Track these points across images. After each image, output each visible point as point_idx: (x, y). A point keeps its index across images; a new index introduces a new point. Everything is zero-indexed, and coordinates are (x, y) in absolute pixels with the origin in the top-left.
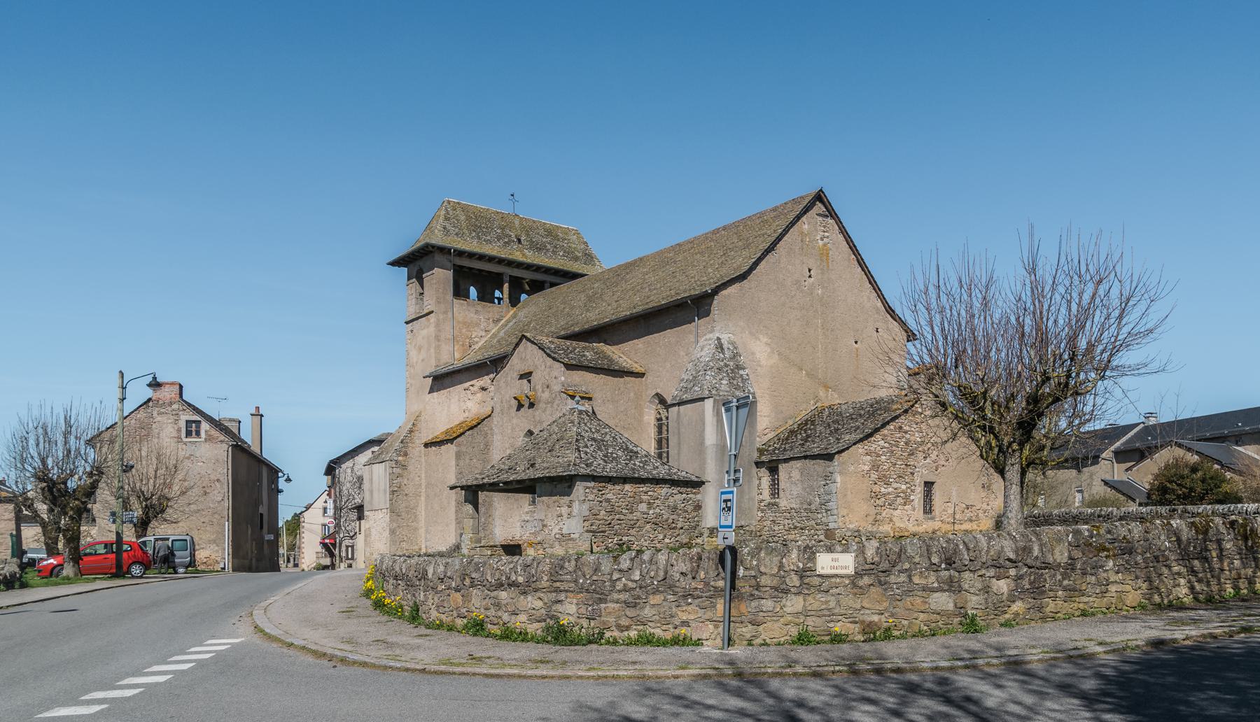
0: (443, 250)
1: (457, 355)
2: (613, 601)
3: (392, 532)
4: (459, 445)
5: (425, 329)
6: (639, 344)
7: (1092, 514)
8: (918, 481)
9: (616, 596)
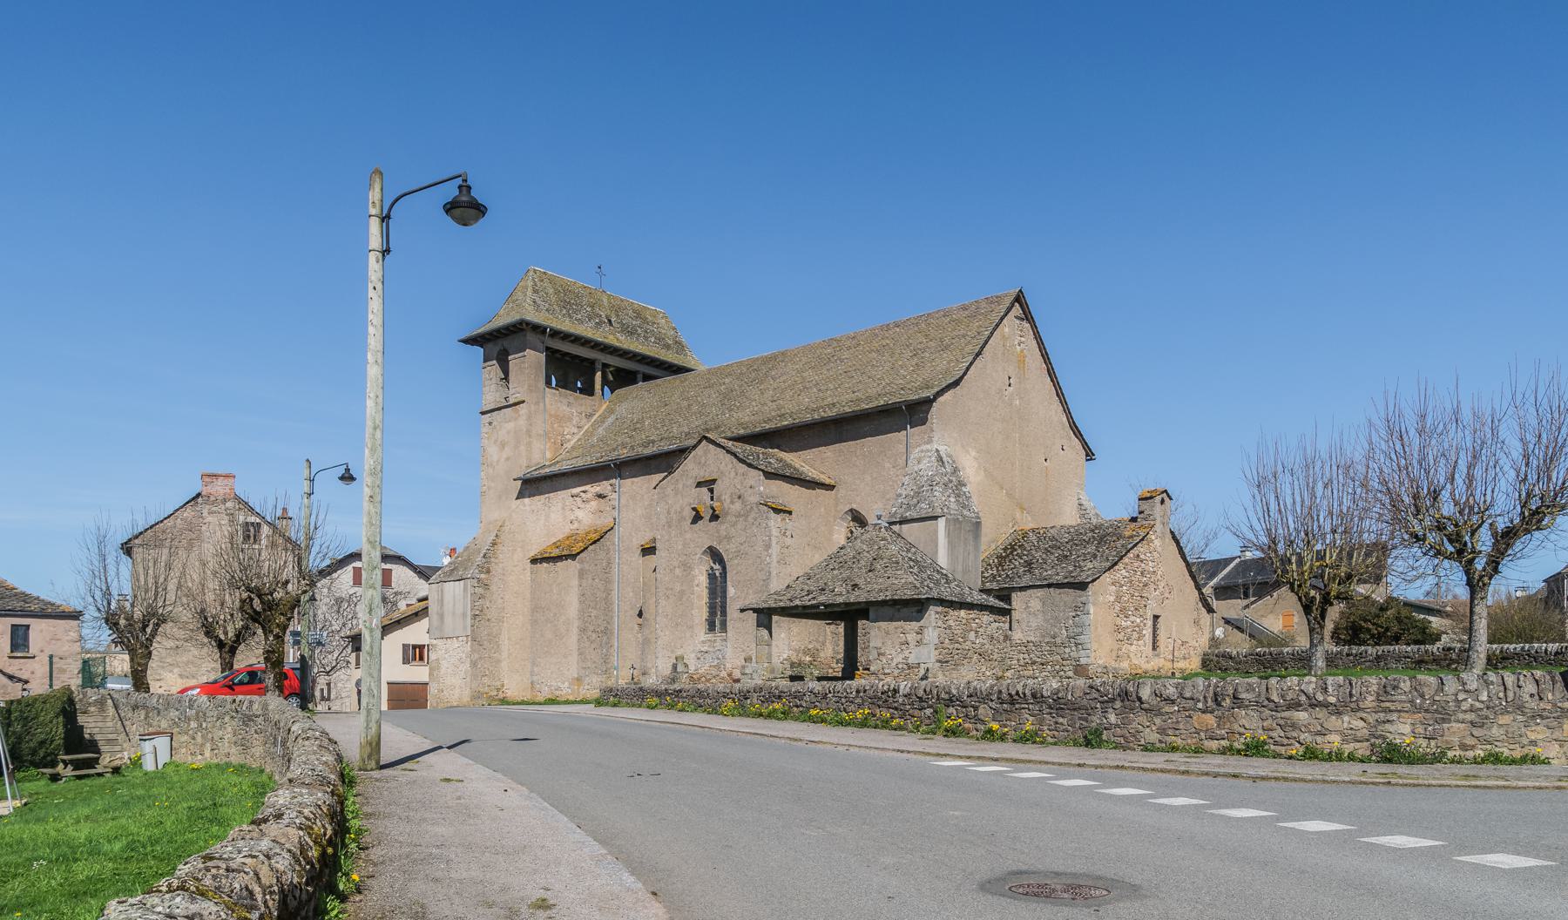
0: (538, 329)
1: (548, 455)
2: (1458, 721)
3: (474, 664)
4: (582, 562)
5: (507, 424)
6: (828, 452)
7: (1340, 653)
8: (1149, 615)
9: (1461, 716)
